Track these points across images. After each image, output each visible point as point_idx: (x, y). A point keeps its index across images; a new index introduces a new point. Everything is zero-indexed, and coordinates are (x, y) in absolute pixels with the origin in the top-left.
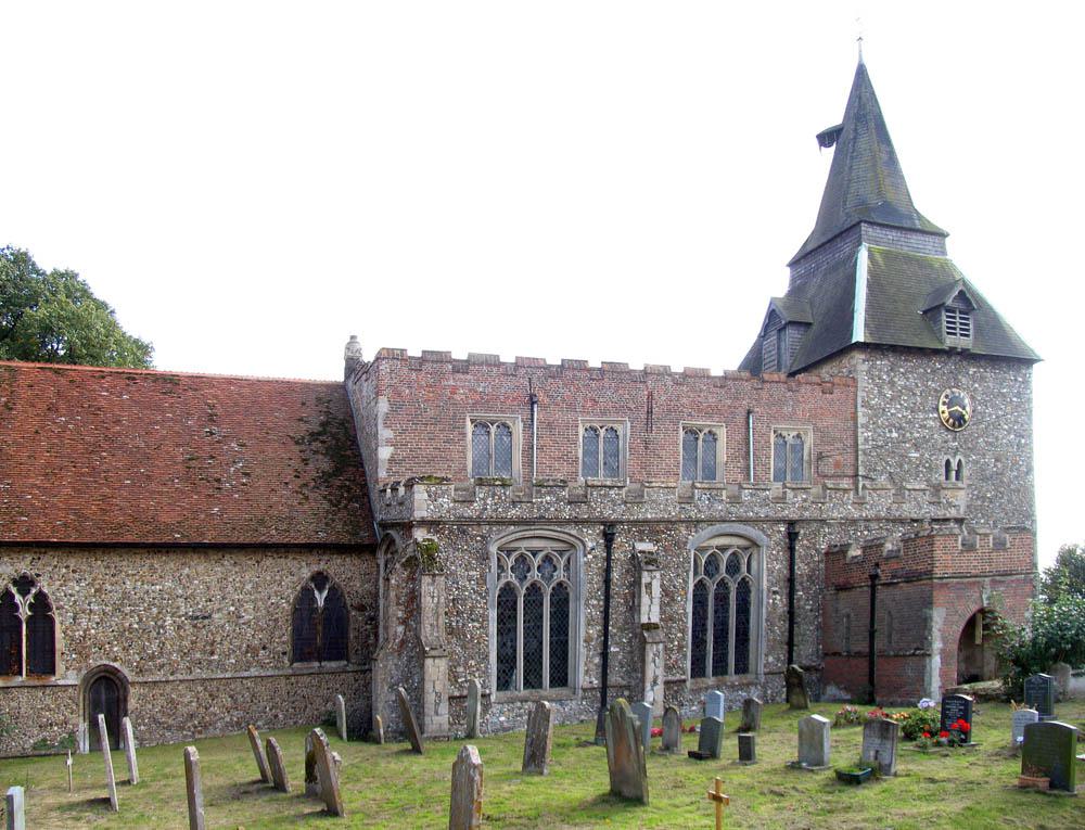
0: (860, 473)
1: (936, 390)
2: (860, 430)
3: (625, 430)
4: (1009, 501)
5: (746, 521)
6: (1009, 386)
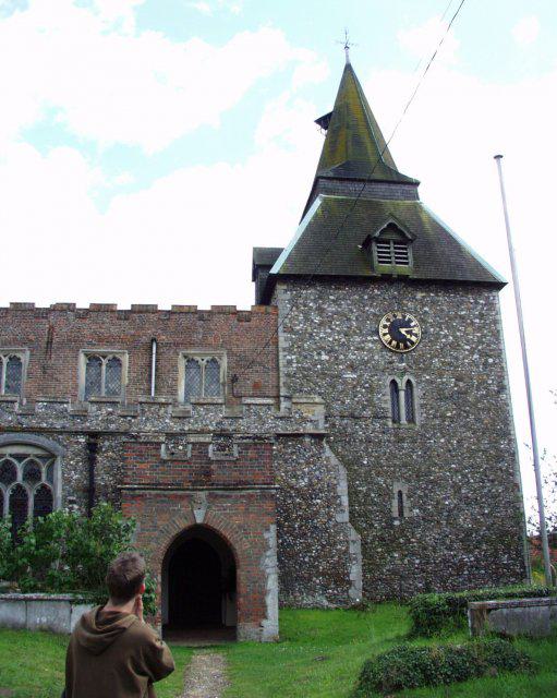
0: (282, 394)
1: (375, 315)
2: (281, 354)
3: (25, 358)
4: (478, 420)
5: (40, 431)
6: (469, 309)
